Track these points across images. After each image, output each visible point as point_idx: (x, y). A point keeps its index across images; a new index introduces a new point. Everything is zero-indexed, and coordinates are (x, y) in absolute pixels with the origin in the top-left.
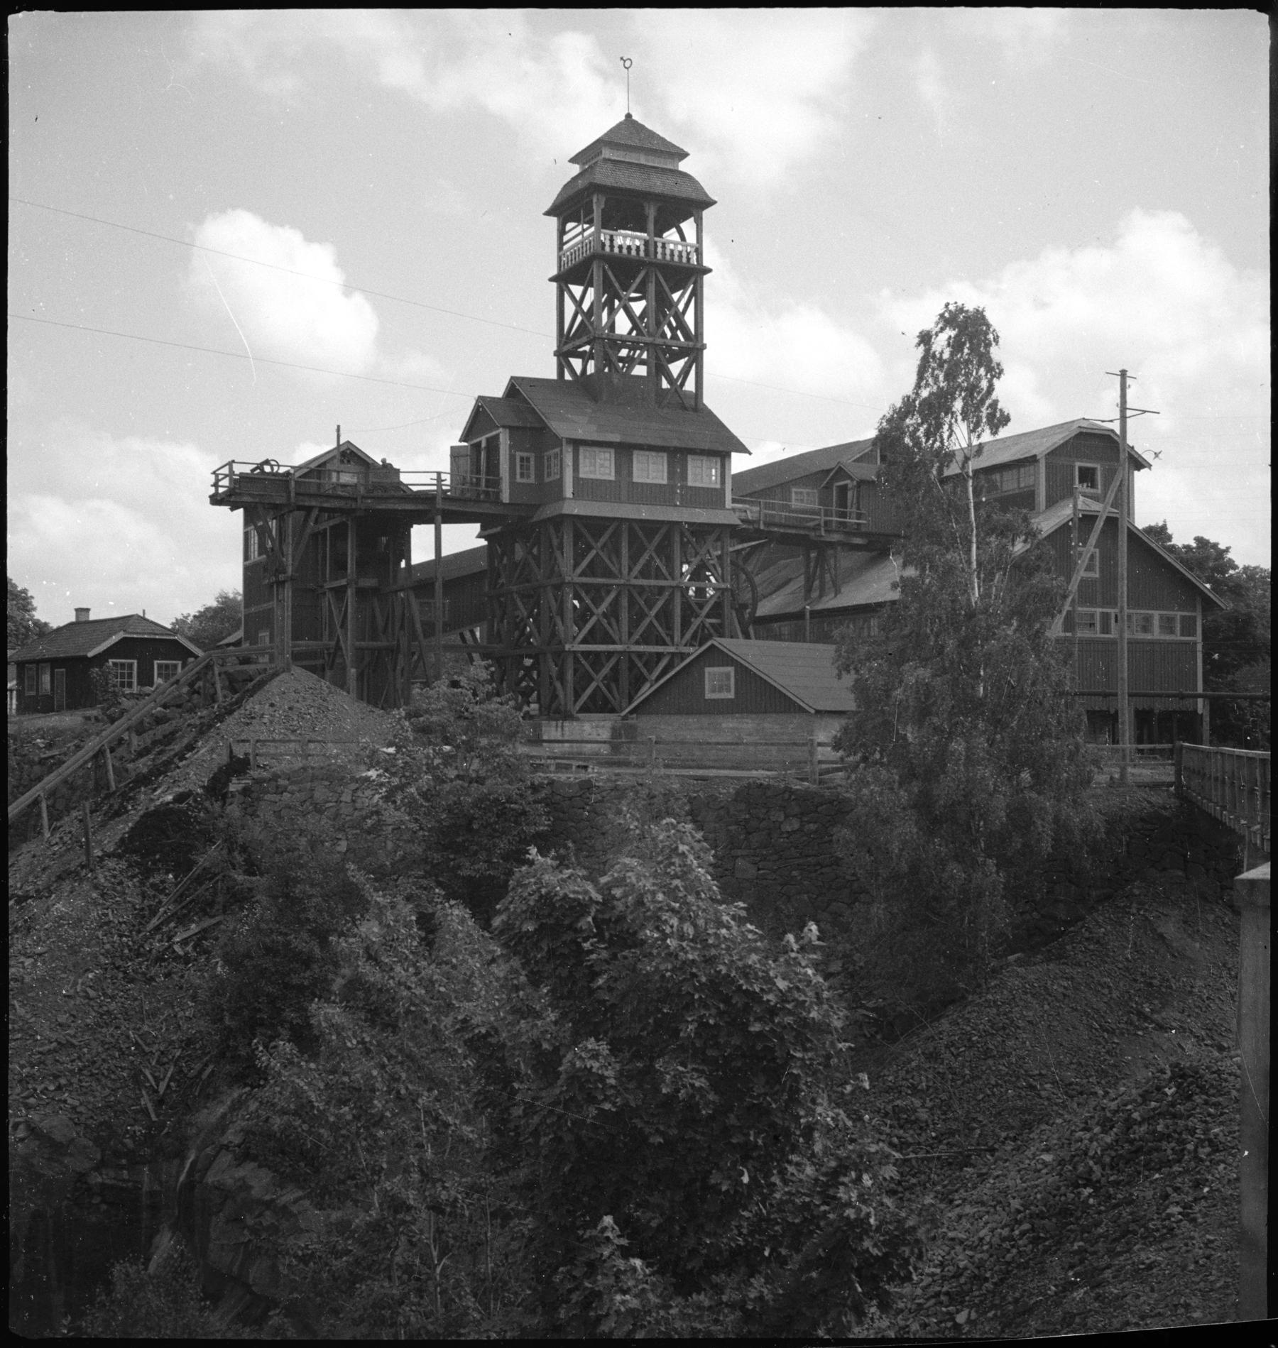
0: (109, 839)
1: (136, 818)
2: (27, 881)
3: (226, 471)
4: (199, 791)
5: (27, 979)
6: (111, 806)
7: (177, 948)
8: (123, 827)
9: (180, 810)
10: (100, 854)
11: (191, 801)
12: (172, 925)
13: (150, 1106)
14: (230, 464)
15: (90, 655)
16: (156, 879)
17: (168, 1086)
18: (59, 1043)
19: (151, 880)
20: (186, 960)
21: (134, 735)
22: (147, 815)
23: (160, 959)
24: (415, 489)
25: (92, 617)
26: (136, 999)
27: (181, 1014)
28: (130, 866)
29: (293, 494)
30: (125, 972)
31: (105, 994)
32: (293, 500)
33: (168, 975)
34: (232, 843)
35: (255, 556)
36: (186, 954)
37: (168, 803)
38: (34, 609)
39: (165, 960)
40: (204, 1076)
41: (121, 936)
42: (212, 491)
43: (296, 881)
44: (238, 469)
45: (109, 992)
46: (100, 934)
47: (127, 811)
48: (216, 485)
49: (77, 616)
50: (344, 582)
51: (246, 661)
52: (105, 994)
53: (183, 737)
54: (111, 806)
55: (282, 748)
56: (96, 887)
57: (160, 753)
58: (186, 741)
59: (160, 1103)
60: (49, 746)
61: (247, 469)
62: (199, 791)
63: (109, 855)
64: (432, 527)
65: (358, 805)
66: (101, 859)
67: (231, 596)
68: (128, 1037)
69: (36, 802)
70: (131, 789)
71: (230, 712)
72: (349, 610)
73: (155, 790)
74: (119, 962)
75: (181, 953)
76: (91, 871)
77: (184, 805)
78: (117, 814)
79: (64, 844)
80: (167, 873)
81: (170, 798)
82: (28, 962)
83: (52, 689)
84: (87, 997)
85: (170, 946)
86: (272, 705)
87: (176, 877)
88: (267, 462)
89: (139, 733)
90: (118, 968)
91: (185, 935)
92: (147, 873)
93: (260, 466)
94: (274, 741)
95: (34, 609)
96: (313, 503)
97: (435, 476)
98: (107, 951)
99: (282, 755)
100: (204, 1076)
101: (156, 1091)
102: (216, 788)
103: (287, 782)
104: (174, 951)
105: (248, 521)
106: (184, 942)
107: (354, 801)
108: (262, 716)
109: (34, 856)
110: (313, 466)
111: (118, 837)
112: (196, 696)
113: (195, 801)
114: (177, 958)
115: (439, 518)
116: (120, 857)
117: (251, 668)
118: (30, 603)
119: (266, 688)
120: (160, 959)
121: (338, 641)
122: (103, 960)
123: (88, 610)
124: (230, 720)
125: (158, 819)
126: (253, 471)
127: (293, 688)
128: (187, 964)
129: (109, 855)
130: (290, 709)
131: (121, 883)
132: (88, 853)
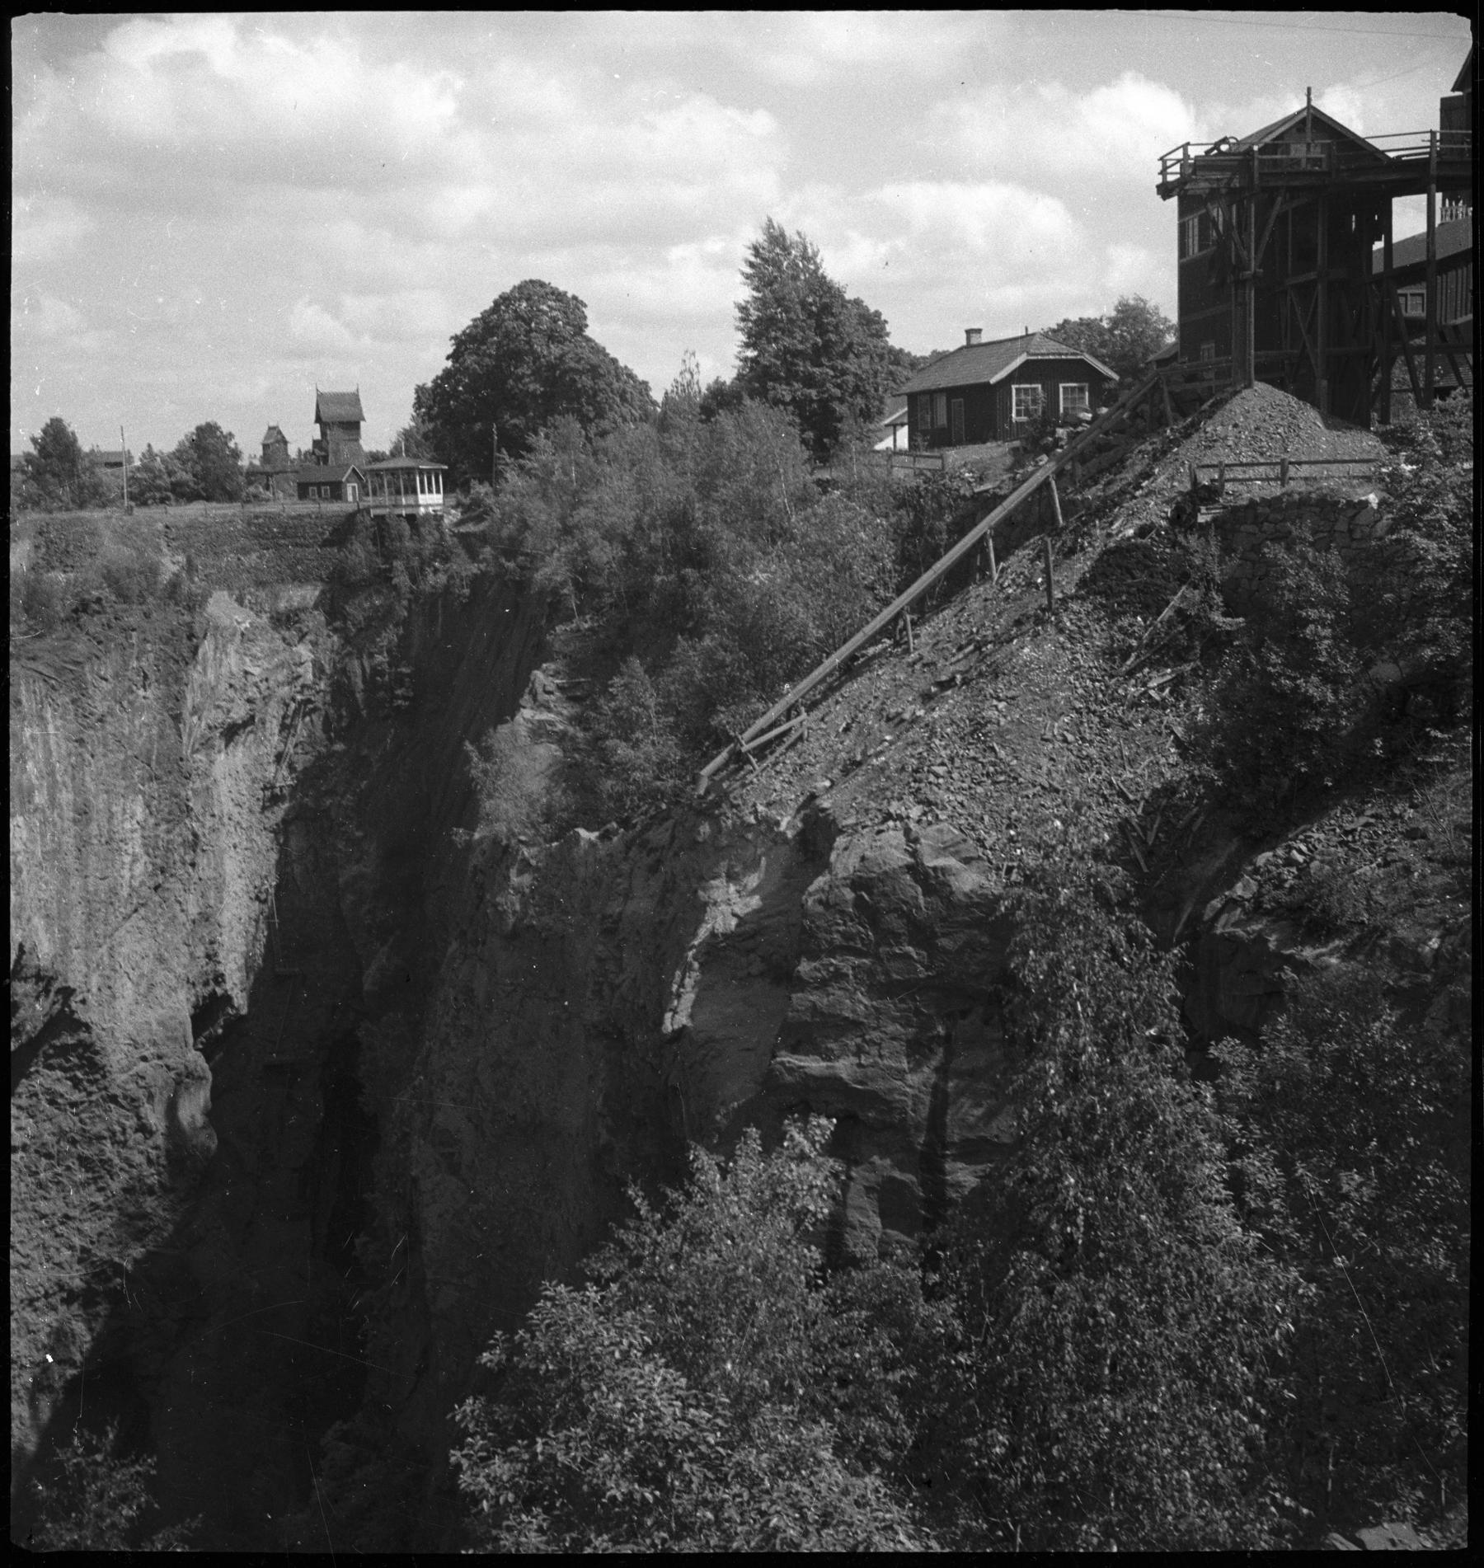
0: (1067, 580)
1: (1096, 557)
2: (983, 625)
3: (1179, 155)
4: (1163, 523)
5: (1003, 721)
6: (1064, 543)
7: (1152, 692)
8: (1082, 565)
9: (1145, 547)
10: (1060, 596)
11: (1153, 534)
12: (1146, 670)
13: (1139, 856)
14: (1185, 146)
15: (993, 381)
16: (1124, 622)
17: (1157, 837)
18: (1043, 788)
19: (1120, 623)
20: (1161, 705)
21: (1078, 466)
22: (1108, 552)
23: (1135, 704)
24: (1392, 155)
25: (985, 338)
26: (1114, 744)
27: (1163, 761)
28: (1095, 608)
29: (1256, 175)
30: (1101, 717)
31: (1083, 739)
32: (1256, 182)
33: (1145, 721)
34: (1208, 582)
35: (1194, 250)
36: (1163, 699)
37: (1129, 538)
38: (888, 334)
39: (1140, 705)
40: (1195, 828)
41: (1093, 681)
42: (1159, 179)
43: (1307, 622)
44: (1193, 152)
45: (1087, 736)
46: (1071, 678)
47: (1083, 549)
48: (1163, 172)
49: (968, 339)
50: (1312, 276)
51: (1191, 378)
52: (1083, 739)
53: (1133, 464)
54: (1064, 543)
55: (1251, 473)
56: (1061, 631)
57: (1109, 483)
58: (1138, 468)
59: (1149, 854)
60: (981, 480)
61: (1200, 151)
62: (1163, 523)
63: (1073, 598)
64: (1424, 197)
65: (1358, 535)
66: (1064, 601)
67: (1132, 302)
68: (1111, 783)
69: (983, 538)
70: (1085, 524)
71: (1188, 436)
72: (1320, 309)
73: (1111, 524)
74: (1093, 707)
75: (1158, 698)
76: (1055, 614)
77: (1147, 541)
78: (1072, 551)
79: (1018, 585)
80: (1135, 616)
81: (1131, 532)
82: (1001, 705)
83: (949, 419)
84: (1065, 740)
85: (1145, 692)
86: (1236, 426)
87: (1145, 620)
88: (1224, 140)
89: (1083, 462)
90: (1094, 712)
91: (1161, 680)
92: (1114, 616)
93: (1217, 145)
94: (1241, 464)
95: (888, 334)
96: (1280, 183)
97: (1428, 136)
98: (1082, 696)
99: (1250, 479)
100: (1195, 828)
101: (1145, 842)
102: (1182, 518)
103: (1267, 510)
104: (1150, 697)
105: (1183, 212)
106: (1161, 688)
107: (1351, 531)
108: (1225, 438)
109: (986, 600)
110: (1267, 140)
111: (1076, 578)
112: (1139, 421)
113: (1158, 534)
114: (1154, 704)
115: (1434, 187)
116: (1083, 599)
117: (1198, 386)
118: (883, 329)
119: (1228, 406)
120: (1135, 704)
121: (1304, 346)
122: (1078, 705)
123: (979, 331)
124: (1187, 444)
125: (1117, 559)
126: (1207, 152)
127: (1259, 403)
128: (1164, 709)
129: (1073, 598)
130: (1257, 429)
131: (1087, 627)
132: (1050, 596)
